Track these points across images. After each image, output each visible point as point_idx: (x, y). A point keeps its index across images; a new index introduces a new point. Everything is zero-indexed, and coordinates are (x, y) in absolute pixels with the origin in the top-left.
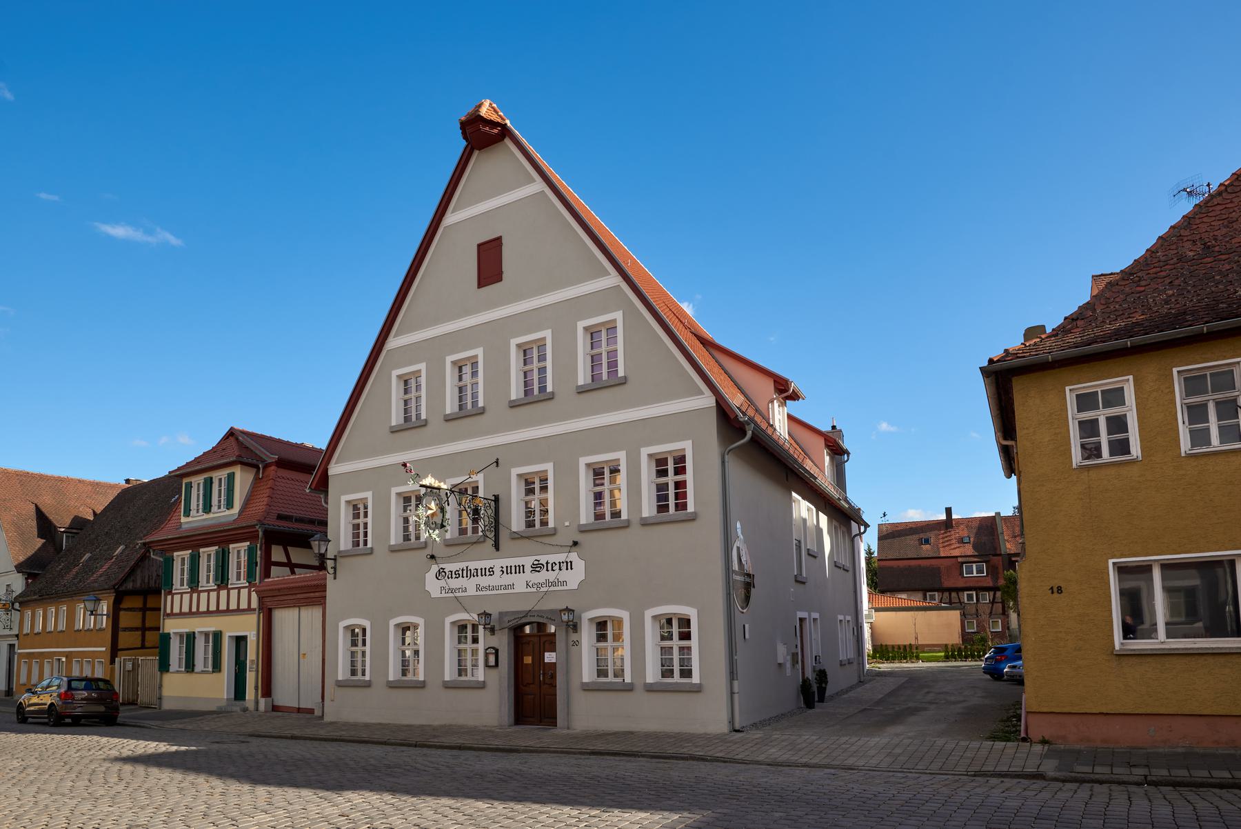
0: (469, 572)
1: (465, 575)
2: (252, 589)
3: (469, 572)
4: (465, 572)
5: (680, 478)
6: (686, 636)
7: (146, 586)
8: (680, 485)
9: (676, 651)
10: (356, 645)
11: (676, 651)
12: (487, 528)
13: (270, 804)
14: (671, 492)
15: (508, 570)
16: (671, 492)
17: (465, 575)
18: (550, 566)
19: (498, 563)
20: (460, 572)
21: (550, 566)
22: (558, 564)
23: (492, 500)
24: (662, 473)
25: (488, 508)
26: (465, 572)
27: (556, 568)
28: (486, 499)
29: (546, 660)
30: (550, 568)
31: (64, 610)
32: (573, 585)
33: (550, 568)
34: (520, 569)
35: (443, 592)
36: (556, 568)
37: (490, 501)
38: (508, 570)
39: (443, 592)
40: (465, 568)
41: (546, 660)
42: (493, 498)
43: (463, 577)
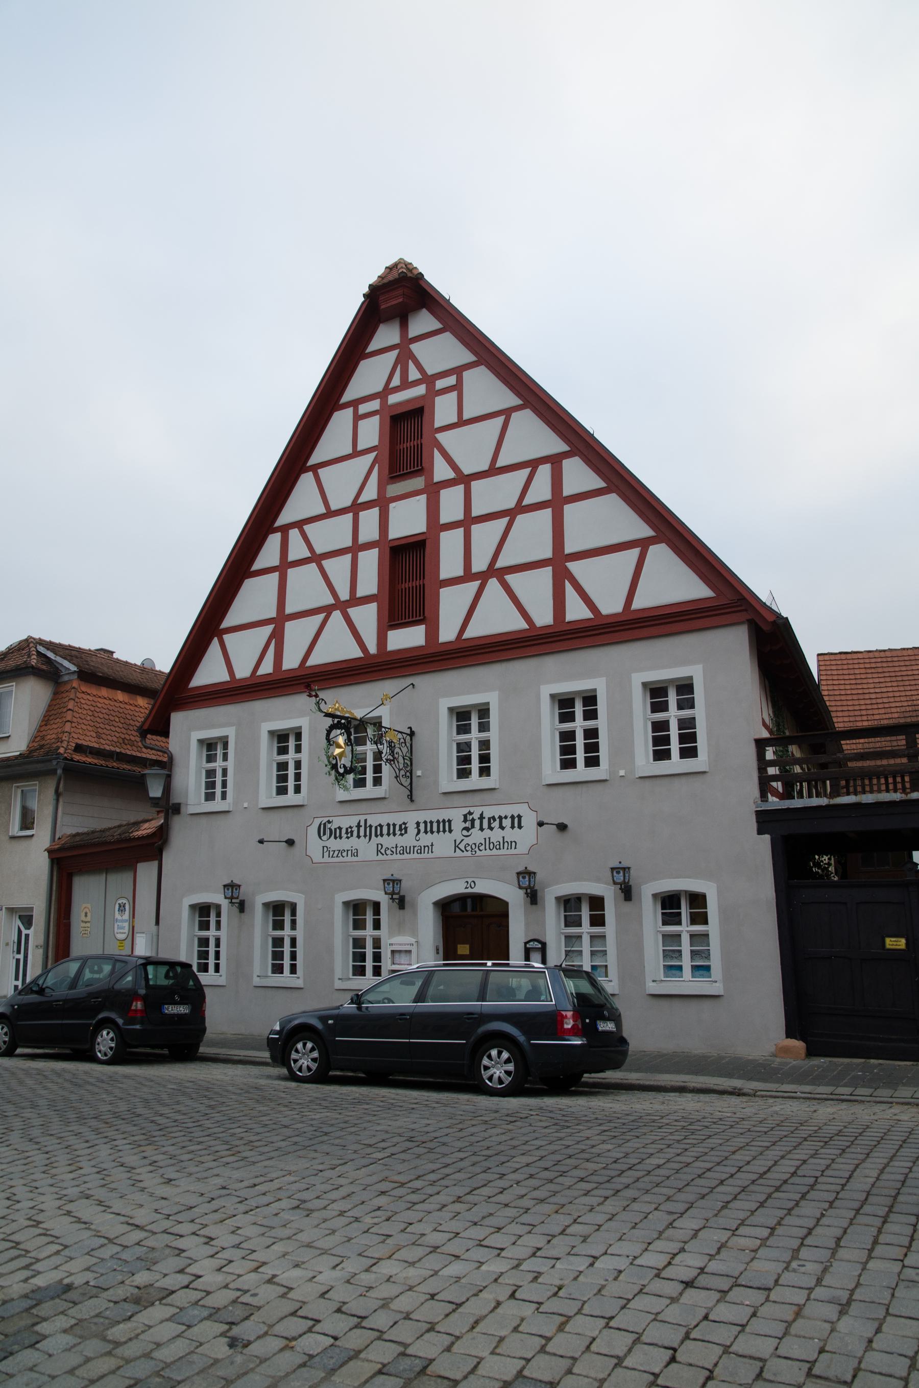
0: (368, 829)
1: (362, 833)
2: (805, 766)
3: (368, 829)
4: (362, 829)
5: (590, 724)
6: (700, 918)
7: (373, 649)
8: (591, 734)
9: (685, 939)
10: (282, 928)
11: (685, 939)
12: (402, 773)
13: (270, 1281)
14: (580, 742)
15: (428, 827)
16: (580, 742)
17: (362, 833)
18: (485, 822)
19: (412, 818)
20: (355, 829)
21: (485, 822)
22: (498, 820)
23: (408, 734)
24: (566, 717)
25: (403, 745)
26: (362, 829)
27: (496, 824)
28: (401, 733)
29: (468, 946)
30: (485, 825)
31: (494, 965)
32: (522, 849)
33: (485, 825)
34: (445, 826)
35: (326, 854)
36: (496, 824)
37: (405, 736)
38: (428, 827)
39: (326, 854)
40: (362, 823)
41: (468, 946)
42: (408, 731)
43: (359, 837)
